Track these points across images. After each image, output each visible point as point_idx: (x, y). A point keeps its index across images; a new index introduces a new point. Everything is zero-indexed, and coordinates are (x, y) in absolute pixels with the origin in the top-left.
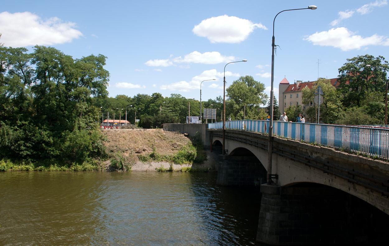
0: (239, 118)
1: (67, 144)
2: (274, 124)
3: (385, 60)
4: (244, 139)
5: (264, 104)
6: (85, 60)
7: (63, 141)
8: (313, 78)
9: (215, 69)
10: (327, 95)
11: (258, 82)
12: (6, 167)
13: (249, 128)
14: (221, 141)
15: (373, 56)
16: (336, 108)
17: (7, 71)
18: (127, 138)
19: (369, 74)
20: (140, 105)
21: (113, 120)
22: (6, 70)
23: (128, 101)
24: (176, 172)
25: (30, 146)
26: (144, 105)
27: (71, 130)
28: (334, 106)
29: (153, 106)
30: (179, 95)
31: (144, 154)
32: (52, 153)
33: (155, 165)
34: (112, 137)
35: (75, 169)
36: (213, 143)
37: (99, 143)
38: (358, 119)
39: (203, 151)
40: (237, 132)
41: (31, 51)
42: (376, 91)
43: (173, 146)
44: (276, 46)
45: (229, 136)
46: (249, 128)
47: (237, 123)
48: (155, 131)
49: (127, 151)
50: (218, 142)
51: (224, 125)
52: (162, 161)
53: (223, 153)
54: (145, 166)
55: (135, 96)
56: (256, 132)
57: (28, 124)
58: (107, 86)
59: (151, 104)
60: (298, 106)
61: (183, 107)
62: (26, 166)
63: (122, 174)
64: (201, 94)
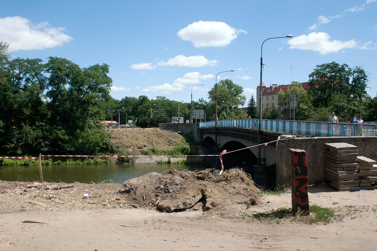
0: (222, 118)
1: (80, 141)
2: (262, 121)
3: (348, 67)
4: (236, 134)
5: (242, 105)
6: (91, 68)
7: (77, 138)
8: (287, 82)
9: (199, 72)
10: (299, 97)
11: (237, 85)
12: (29, 162)
13: (241, 125)
14: (213, 137)
15: (338, 63)
16: (307, 109)
17: (24, 80)
18: (129, 136)
19: (335, 79)
20: (128, 107)
21: (111, 121)
22: (23, 78)
23: (115, 103)
24: (174, 164)
25: (48, 144)
26: (132, 107)
27: (82, 129)
28: (305, 107)
29: (141, 107)
30: (164, 97)
31: (145, 149)
32: (68, 149)
33: (156, 158)
34: (116, 136)
35: (88, 162)
36: (203, 139)
37: (106, 140)
38: (325, 118)
39: (195, 146)
40: (229, 129)
41: (45, 61)
42: (341, 94)
43: (169, 143)
44: (263, 65)
45: (220, 133)
46: (241, 125)
47: (229, 122)
48: (153, 130)
49: (130, 147)
50: (209, 139)
51: (216, 123)
52: (161, 155)
53: (215, 147)
54: (146, 159)
55: (123, 99)
56: (247, 128)
57: (45, 125)
58: (110, 91)
59: (140, 106)
60: (273, 107)
61: (169, 108)
62: (46, 161)
63: (128, 167)
64: (192, 97)
